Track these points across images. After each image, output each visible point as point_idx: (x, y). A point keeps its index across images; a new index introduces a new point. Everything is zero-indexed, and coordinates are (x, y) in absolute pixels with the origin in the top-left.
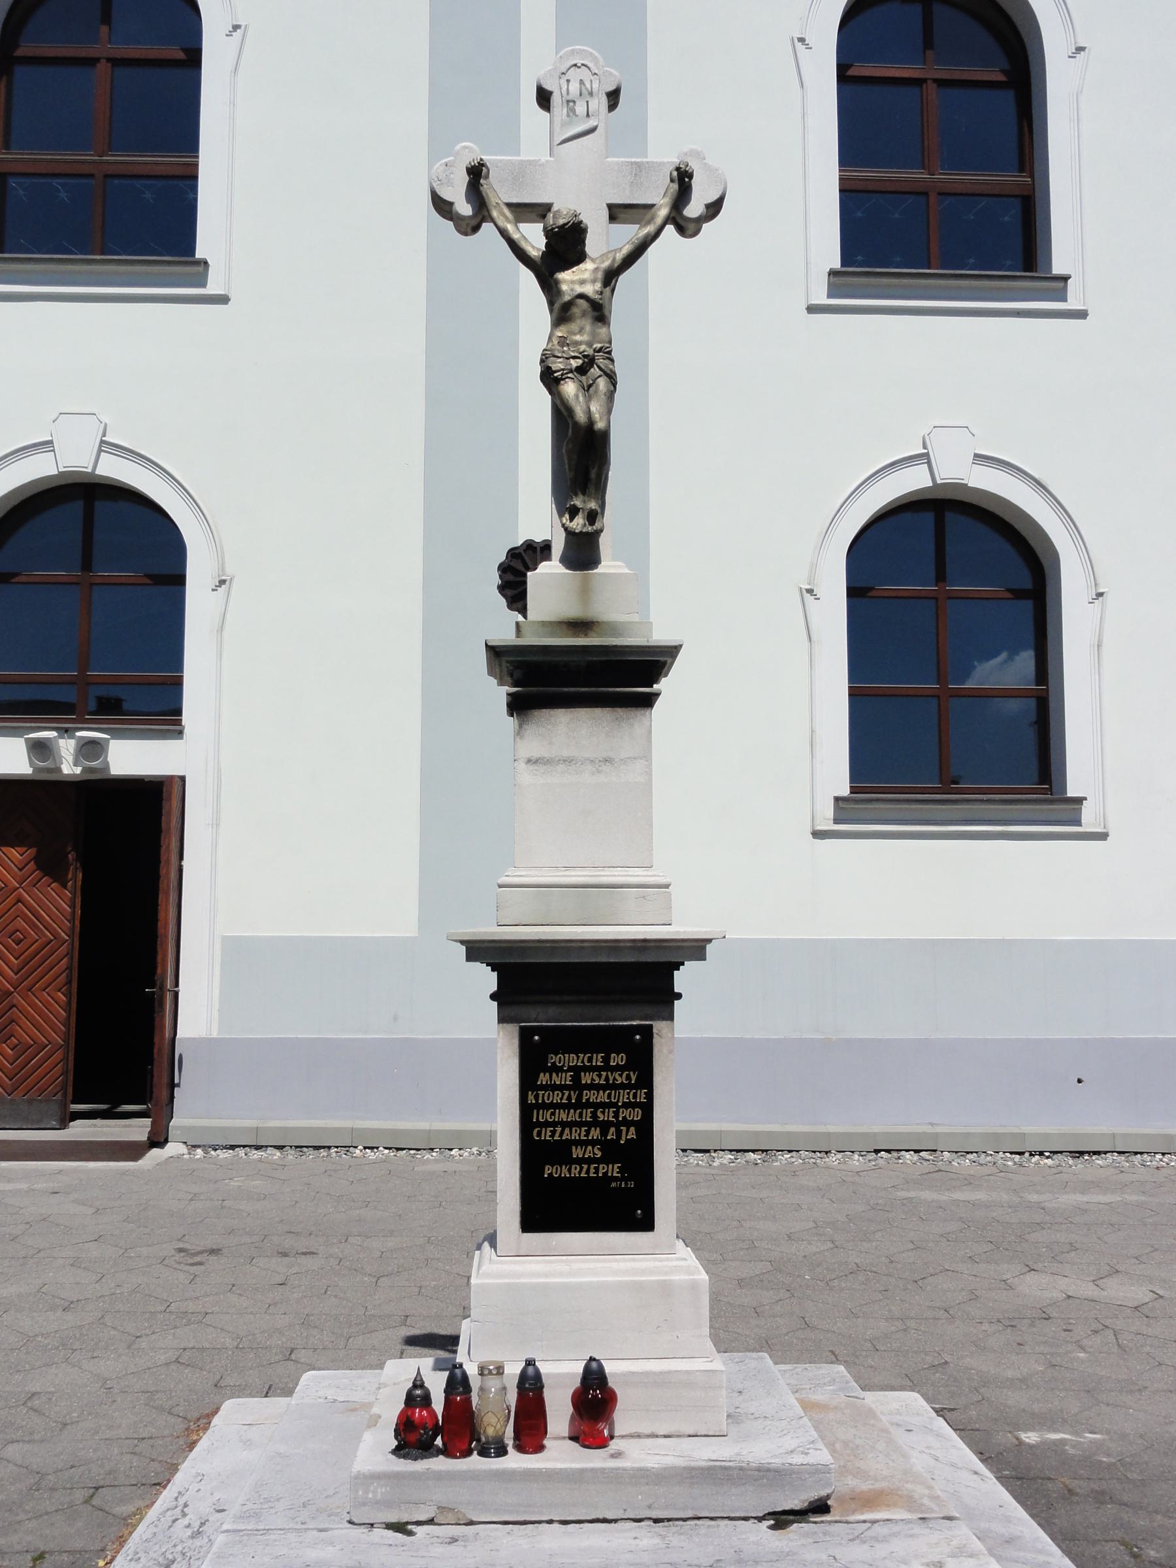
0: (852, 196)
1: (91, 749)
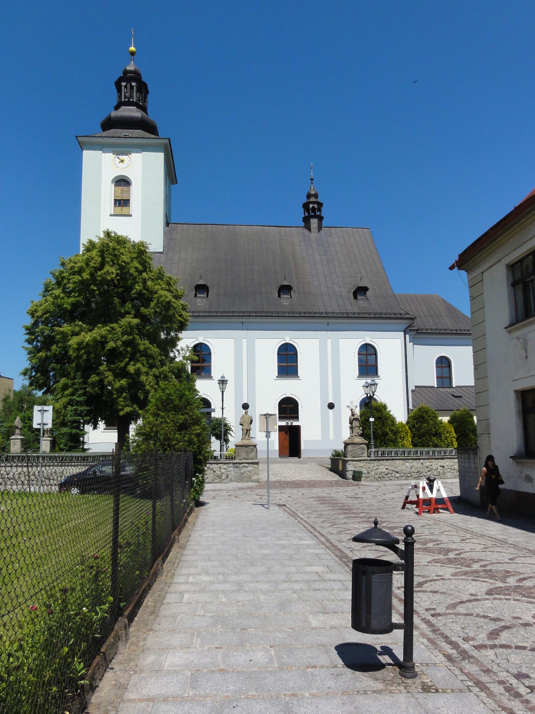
0: (279, 367)
1: (292, 423)
